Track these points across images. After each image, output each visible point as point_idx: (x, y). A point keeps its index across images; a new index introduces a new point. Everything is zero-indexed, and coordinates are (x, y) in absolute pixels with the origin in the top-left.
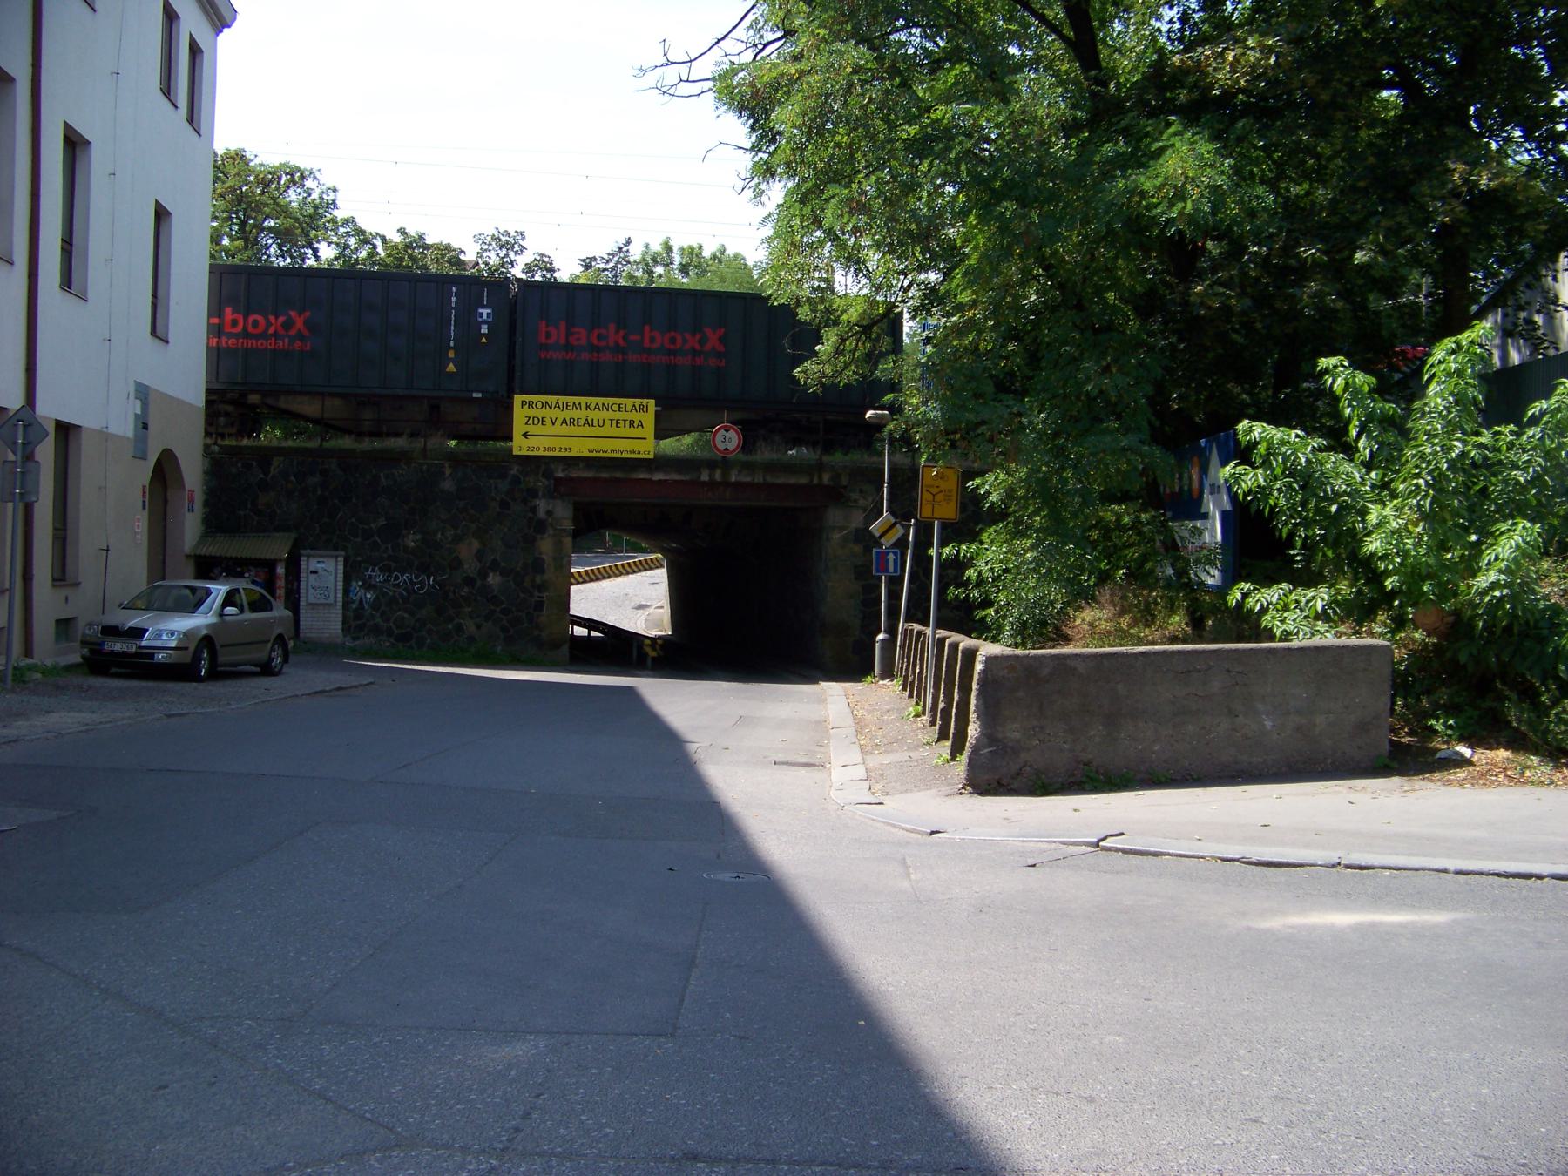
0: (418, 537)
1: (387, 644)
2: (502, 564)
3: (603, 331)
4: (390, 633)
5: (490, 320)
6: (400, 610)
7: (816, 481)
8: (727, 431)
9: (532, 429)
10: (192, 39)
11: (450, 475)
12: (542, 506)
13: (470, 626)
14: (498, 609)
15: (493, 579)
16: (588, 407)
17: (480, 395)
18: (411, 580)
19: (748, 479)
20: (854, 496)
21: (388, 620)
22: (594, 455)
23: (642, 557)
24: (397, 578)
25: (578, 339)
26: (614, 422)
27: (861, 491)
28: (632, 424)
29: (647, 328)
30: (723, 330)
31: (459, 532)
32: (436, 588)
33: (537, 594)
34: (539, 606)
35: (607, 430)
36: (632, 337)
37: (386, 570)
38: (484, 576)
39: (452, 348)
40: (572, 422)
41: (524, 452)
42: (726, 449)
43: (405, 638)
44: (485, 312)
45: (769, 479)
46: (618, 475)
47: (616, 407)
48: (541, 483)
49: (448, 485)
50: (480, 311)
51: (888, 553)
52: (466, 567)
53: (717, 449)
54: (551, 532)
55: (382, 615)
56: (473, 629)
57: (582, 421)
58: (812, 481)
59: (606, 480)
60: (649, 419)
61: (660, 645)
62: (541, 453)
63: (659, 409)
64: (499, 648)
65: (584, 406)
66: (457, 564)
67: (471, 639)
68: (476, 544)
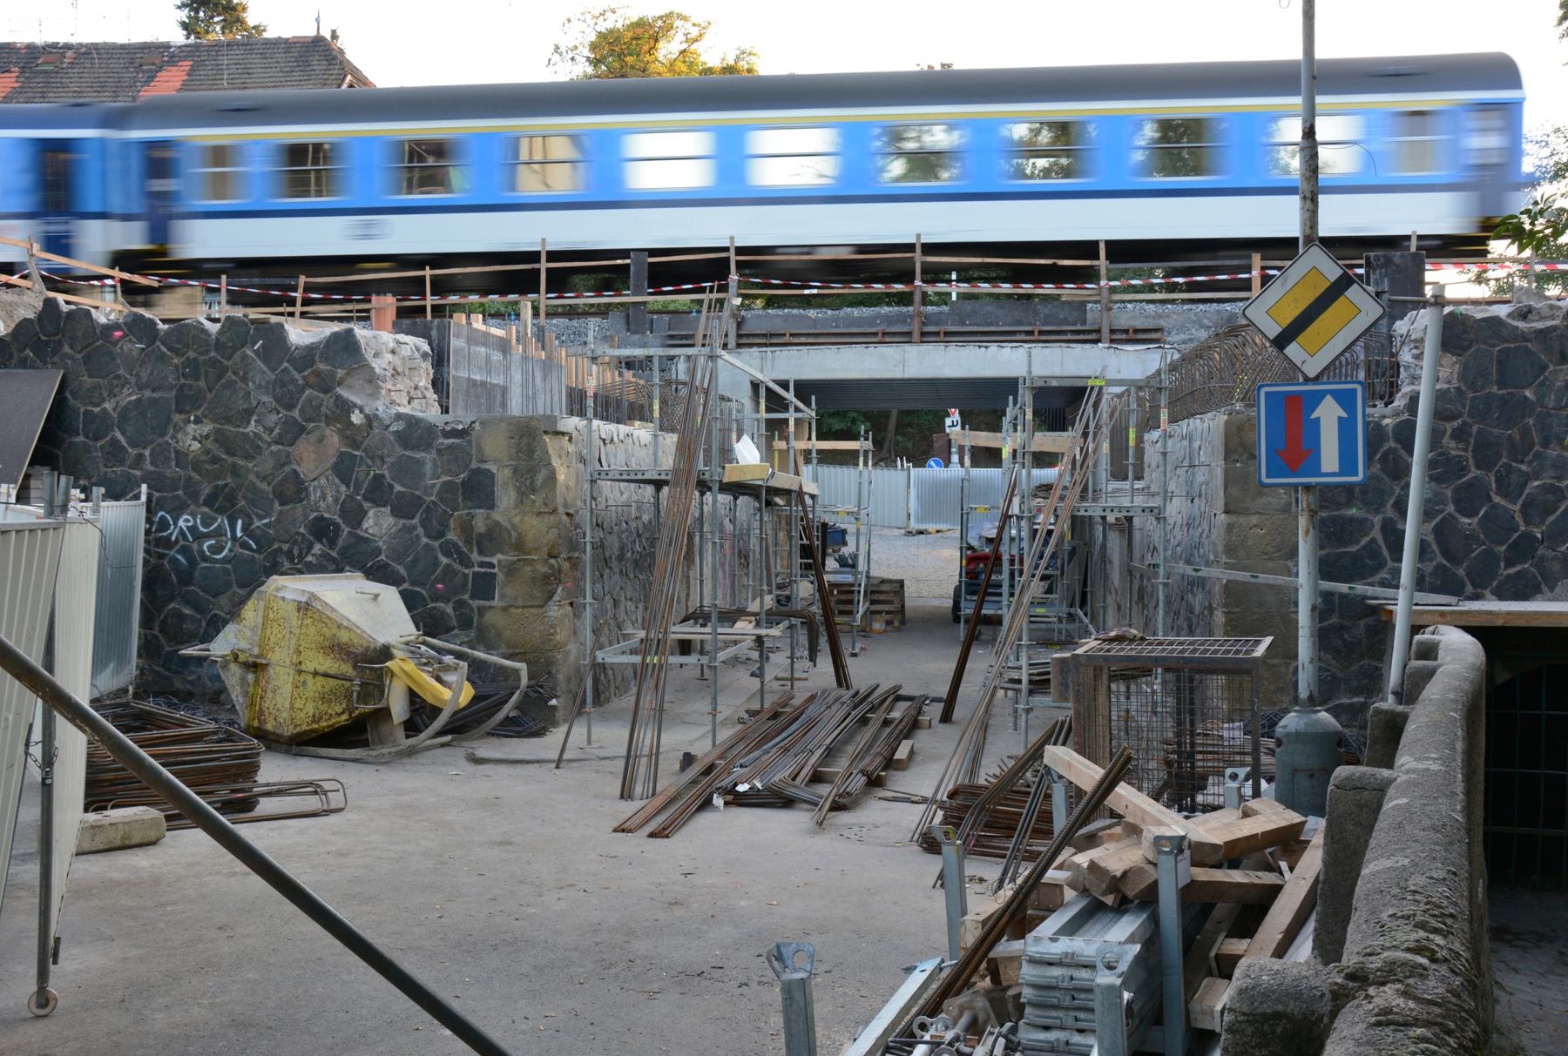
0: (207, 428)
10: (776, 382)
18: (193, 529)
23: (1080, 766)
31: (296, 413)
32: (249, 548)
38: (355, 516)
52: (314, 496)
66: (293, 490)
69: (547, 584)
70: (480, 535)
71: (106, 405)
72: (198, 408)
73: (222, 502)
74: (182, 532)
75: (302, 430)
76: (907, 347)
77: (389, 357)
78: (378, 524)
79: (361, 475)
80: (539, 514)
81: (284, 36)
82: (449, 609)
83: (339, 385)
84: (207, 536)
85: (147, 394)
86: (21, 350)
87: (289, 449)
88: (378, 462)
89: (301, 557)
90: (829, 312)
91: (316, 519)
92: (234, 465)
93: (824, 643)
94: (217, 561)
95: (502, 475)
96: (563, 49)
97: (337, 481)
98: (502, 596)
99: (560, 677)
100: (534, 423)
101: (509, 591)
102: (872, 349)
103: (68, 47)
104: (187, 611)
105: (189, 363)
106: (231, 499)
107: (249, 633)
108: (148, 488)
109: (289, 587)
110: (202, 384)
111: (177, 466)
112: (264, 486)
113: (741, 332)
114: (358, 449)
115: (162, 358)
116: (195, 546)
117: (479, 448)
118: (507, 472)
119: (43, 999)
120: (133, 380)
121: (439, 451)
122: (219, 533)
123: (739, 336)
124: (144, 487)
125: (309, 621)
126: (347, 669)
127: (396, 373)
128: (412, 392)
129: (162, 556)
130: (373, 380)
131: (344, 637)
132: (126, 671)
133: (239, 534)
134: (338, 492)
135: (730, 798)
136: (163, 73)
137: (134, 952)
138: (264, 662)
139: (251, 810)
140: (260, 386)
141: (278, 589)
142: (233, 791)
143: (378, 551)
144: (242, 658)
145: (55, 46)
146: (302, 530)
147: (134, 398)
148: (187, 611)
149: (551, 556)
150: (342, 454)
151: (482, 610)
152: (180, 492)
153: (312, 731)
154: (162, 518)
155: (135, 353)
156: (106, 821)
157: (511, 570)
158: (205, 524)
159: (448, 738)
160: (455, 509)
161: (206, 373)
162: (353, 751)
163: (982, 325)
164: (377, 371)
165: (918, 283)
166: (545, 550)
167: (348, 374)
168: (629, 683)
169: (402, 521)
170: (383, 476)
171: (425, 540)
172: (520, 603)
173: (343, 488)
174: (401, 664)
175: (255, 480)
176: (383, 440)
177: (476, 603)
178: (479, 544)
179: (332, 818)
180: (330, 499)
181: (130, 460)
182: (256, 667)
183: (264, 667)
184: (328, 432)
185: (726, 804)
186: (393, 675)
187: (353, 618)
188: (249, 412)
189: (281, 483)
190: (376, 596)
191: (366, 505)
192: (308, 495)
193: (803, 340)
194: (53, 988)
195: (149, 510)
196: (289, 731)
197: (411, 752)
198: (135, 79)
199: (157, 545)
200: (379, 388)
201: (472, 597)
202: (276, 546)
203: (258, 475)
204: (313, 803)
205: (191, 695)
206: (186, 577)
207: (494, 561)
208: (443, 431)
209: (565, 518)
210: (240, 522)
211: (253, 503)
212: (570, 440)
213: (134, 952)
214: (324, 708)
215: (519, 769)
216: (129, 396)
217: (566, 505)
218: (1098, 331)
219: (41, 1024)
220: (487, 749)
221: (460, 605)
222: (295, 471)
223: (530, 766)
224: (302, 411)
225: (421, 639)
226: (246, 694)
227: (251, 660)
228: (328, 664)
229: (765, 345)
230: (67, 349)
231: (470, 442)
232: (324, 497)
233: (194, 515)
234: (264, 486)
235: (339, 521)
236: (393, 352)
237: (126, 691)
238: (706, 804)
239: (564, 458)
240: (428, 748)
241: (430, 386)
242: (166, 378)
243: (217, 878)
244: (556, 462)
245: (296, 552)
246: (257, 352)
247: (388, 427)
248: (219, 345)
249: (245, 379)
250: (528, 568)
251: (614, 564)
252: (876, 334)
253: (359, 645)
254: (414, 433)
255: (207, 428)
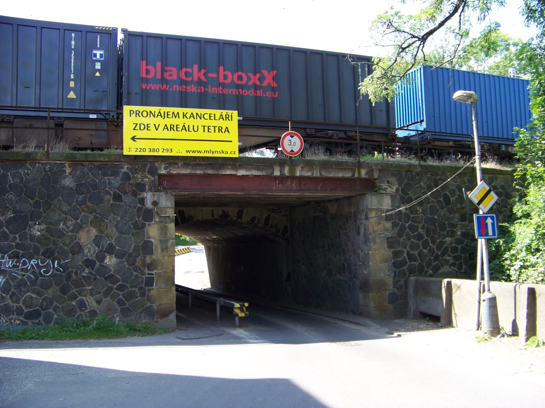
0: (43, 227)
1: (18, 322)
2: (117, 248)
3: (189, 70)
4: (19, 312)
5: (102, 59)
6: (28, 291)
7: (356, 175)
8: (292, 137)
9: (139, 134)
11: (70, 174)
12: (149, 197)
13: (91, 302)
14: (115, 287)
15: (110, 261)
16: (184, 116)
17: (95, 116)
18: (37, 265)
19: (309, 174)
20: (385, 185)
21: (17, 301)
22: (191, 154)
24: (25, 263)
25: (171, 75)
26: (206, 128)
27: (388, 182)
28: (220, 130)
29: (221, 68)
30: (275, 72)
31: (79, 221)
32: (60, 271)
33: (147, 271)
34: (150, 282)
35: (200, 135)
36: (210, 75)
37: (15, 256)
39: (72, 80)
40: (172, 128)
41: (133, 153)
42: (292, 151)
43: (33, 315)
44: (98, 53)
45: (325, 174)
46: (210, 172)
47: (207, 116)
48: (148, 179)
49: (68, 182)
50: (95, 52)
51: (487, 217)
53: (286, 152)
54: (157, 220)
55: (11, 297)
56: (94, 304)
57: (181, 127)
58: (354, 175)
59: (199, 176)
60: (233, 125)
61: (246, 308)
62: (147, 153)
63: (241, 118)
64: (117, 319)
65: (181, 115)
66: (78, 249)
67: (93, 313)
68: (94, 232)
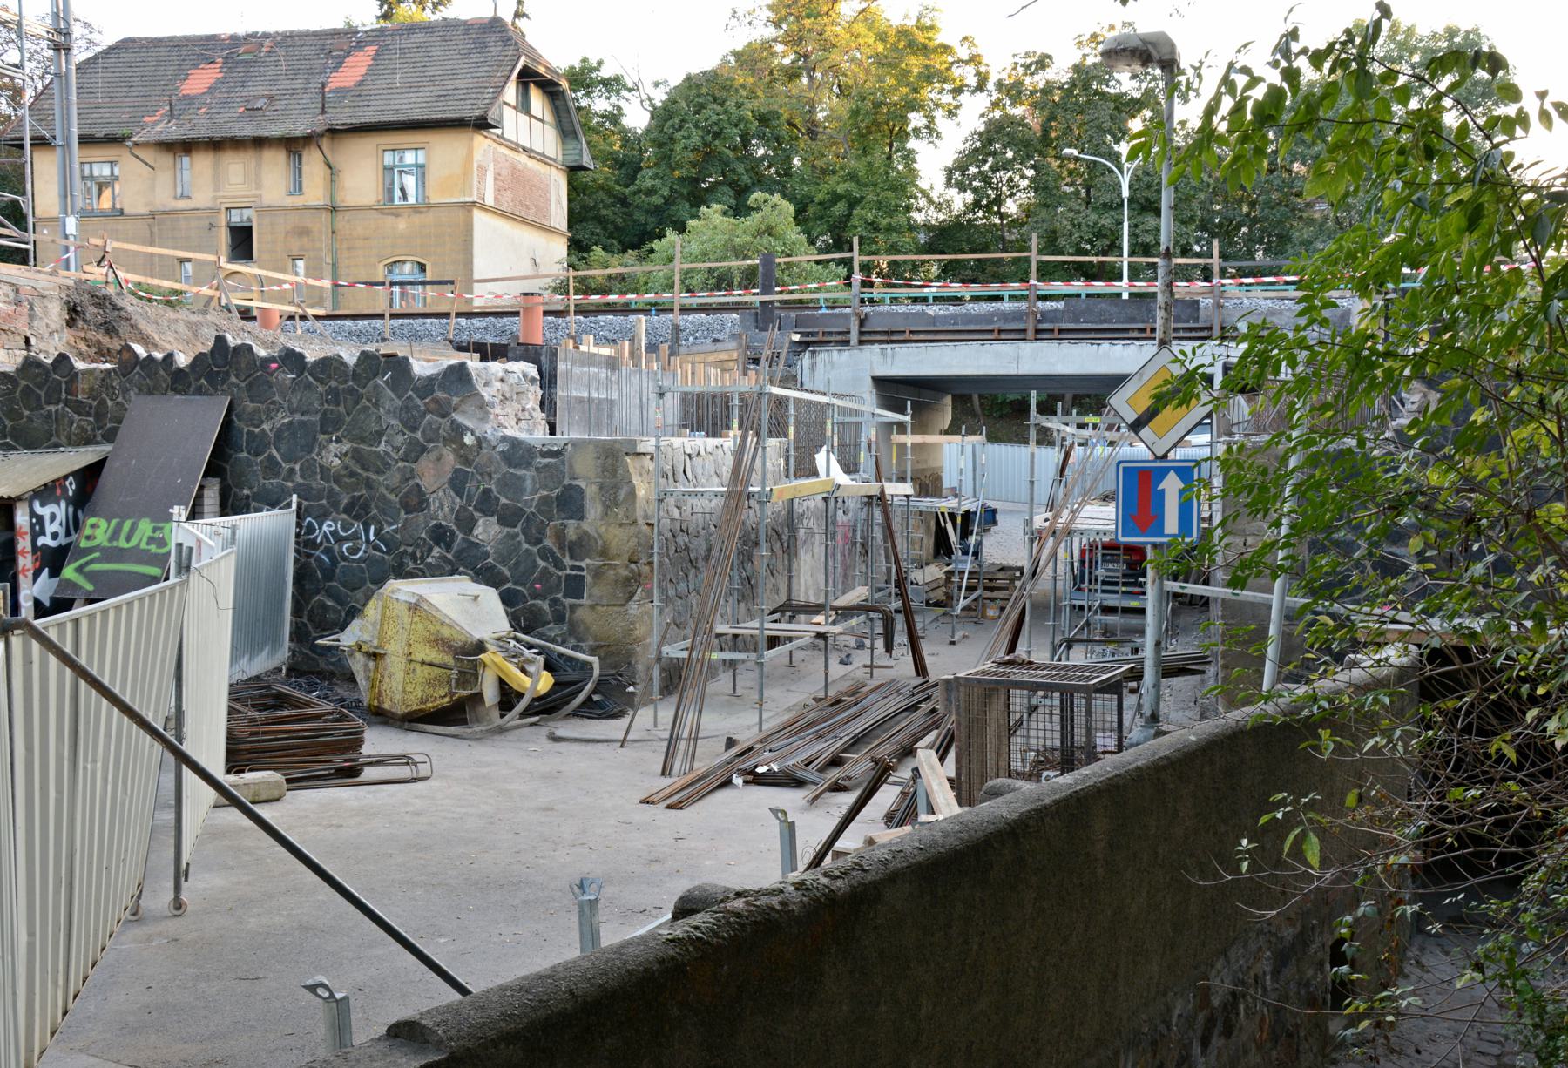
0: (346, 447)
18: (334, 533)
31: (418, 435)
32: (380, 550)
38: (468, 524)
66: (416, 501)
69: (630, 585)
70: (571, 542)
71: (266, 427)
72: (338, 430)
73: (358, 510)
74: (325, 536)
75: (424, 450)
76: (1022, 344)
77: (498, 385)
78: (487, 531)
79: (474, 489)
80: (621, 525)
81: (463, 18)
82: (545, 606)
83: (455, 410)
84: (346, 539)
85: (298, 417)
86: (198, 379)
87: (413, 466)
88: (487, 478)
89: (423, 559)
90: (951, 308)
91: (435, 526)
92: (368, 478)
93: (901, 638)
94: (354, 561)
95: (590, 490)
96: (740, 13)
97: (452, 493)
98: (590, 596)
99: (640, 667)
100: (617, 446)
101: (596, 591)
102: (987, 346)
103: (266, 36)
104: (330, 603)
105: (331, 391)
106: (366, 507)
107: (370, 628)
108: (299, 497)
109: (402, 590)
110: (342, 409)
111: (322, 479)
112: (392, 497)
113: (864, 329)
114: (470, 466)
115: (309, 386)
116: (336, 548)
117: (571, 467)
118: (594, 488)
119: (178, 905)
120: (286, 405)
121: (537, 469)
122: (355, 537)
123: (861, 333)
124: (295, 497)
125: (417, 619)
126: (448, 659)
127: (505, 398)
128: (520, 414)
129: (309, 556)
130: (483, 406)
131: (446, 632)
132: (280, 653)
133: (372, 538)
134: (453, 502)
135: (750, 778)
136: (351, 59)
137: (246, 878)
138: (382, 652)
139: (357, 776)
140: (388, 412)
141: (393, 592)
142: (346, 761)
143: (487, 555)
144: (364, 648)
145: (254, 35)
146: (423, 535)
147: (286, 420)
148: (330, 603)
149: (631, 561)
150: (456, 471)
151: (573, 608)
152: (324, 501)
153: (421, 710)
154: (310, 523)
155: (287, 382)
156: (241, 782)
157: (598, 574)
158: (345, 529)
159: (536, 719)
160: (550, 519)
161: (345, 399)
162: (453, 728)
163: (1096, 322)
164: (487, 398)
165: (1032, 282)
166: (626, 556)
167: (462, 401)
168: (716, 669)
169: (507, 529)
170: (490, 490)
171: (525, 546)
172: (605, 602)
173: (458, 500)
174: (492, 657)
175: (385, 492)
176: (490, 459)
177: (568, 601)
178: (570, 550)
179: (419, 785)
180: (446, 509)
181: (284, 473)
182: (375, 656)
183: (382, 656)
184: (445, 452)
185: (746, 782)
186: (485, 666)
187: (454, 616)
188: (380, 434)
189: (407, 495)
190: (476, 598)
191: (477, 515)
192: (428, 506)
193: (922, 337)
194: (184, 897)
195: (298, 516)
196: (401, 710)
197: (501, 730)
198: (325, 66)
199: (305, 546)
200: (488, 413)
201: (565, 596)
202: (402, 548)
203: (387, 488)
204: (405, 772)
205: (333, 674)
206: (329, 574)
207: (583, 564)
208: (541, 451)
209: (645, 528)
210: (372, 528)
211: (383, 511)
212: (652, 459)
213: (246, 878)
214: (431, 691)
215: (590, 747)
216: (283, 419)
217: (646, 516)
218: (1210, 329)
219: (176, 920)
220: (566, 728)
221: (555, 602)
222: (418, 485)
223: (600, 745)
224: (424, 432)
225: (512, 634)
226: (368, 678)
227: (372, 650)
228: (433, 655)
229: (886, 342)
230: (233, 379)
231: (563, 462)
232: (441, 507)
233: (335, 521)
234: (392, 497)
235: (454, 528)
236: (502, 380)
237: (280, 670)
238: (727, 783)
239: (645, 475)
240: (518, 727)
241: (538, 408)
242: (312, 404)
243: (317, 828)
244: (636, 480)
245: (418, 554)
246: (386, 382)
247: (494, 447)
248: (355, 376)
249: (376, 405)
250: (612, 572)
251: (701, 564)
252: (992, 331)
253: (459, 640)
254: (518, 453)
255: (346, 447)
